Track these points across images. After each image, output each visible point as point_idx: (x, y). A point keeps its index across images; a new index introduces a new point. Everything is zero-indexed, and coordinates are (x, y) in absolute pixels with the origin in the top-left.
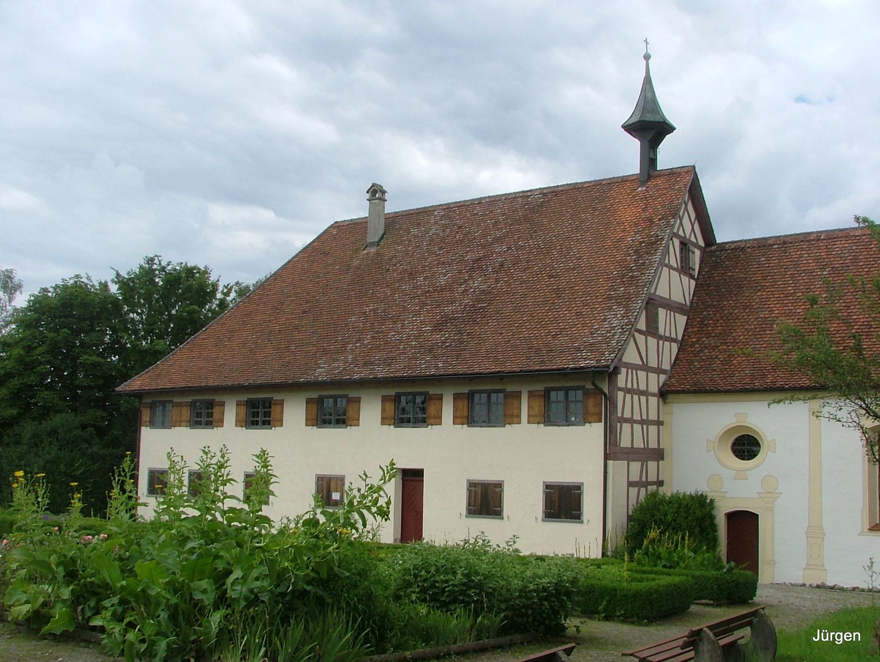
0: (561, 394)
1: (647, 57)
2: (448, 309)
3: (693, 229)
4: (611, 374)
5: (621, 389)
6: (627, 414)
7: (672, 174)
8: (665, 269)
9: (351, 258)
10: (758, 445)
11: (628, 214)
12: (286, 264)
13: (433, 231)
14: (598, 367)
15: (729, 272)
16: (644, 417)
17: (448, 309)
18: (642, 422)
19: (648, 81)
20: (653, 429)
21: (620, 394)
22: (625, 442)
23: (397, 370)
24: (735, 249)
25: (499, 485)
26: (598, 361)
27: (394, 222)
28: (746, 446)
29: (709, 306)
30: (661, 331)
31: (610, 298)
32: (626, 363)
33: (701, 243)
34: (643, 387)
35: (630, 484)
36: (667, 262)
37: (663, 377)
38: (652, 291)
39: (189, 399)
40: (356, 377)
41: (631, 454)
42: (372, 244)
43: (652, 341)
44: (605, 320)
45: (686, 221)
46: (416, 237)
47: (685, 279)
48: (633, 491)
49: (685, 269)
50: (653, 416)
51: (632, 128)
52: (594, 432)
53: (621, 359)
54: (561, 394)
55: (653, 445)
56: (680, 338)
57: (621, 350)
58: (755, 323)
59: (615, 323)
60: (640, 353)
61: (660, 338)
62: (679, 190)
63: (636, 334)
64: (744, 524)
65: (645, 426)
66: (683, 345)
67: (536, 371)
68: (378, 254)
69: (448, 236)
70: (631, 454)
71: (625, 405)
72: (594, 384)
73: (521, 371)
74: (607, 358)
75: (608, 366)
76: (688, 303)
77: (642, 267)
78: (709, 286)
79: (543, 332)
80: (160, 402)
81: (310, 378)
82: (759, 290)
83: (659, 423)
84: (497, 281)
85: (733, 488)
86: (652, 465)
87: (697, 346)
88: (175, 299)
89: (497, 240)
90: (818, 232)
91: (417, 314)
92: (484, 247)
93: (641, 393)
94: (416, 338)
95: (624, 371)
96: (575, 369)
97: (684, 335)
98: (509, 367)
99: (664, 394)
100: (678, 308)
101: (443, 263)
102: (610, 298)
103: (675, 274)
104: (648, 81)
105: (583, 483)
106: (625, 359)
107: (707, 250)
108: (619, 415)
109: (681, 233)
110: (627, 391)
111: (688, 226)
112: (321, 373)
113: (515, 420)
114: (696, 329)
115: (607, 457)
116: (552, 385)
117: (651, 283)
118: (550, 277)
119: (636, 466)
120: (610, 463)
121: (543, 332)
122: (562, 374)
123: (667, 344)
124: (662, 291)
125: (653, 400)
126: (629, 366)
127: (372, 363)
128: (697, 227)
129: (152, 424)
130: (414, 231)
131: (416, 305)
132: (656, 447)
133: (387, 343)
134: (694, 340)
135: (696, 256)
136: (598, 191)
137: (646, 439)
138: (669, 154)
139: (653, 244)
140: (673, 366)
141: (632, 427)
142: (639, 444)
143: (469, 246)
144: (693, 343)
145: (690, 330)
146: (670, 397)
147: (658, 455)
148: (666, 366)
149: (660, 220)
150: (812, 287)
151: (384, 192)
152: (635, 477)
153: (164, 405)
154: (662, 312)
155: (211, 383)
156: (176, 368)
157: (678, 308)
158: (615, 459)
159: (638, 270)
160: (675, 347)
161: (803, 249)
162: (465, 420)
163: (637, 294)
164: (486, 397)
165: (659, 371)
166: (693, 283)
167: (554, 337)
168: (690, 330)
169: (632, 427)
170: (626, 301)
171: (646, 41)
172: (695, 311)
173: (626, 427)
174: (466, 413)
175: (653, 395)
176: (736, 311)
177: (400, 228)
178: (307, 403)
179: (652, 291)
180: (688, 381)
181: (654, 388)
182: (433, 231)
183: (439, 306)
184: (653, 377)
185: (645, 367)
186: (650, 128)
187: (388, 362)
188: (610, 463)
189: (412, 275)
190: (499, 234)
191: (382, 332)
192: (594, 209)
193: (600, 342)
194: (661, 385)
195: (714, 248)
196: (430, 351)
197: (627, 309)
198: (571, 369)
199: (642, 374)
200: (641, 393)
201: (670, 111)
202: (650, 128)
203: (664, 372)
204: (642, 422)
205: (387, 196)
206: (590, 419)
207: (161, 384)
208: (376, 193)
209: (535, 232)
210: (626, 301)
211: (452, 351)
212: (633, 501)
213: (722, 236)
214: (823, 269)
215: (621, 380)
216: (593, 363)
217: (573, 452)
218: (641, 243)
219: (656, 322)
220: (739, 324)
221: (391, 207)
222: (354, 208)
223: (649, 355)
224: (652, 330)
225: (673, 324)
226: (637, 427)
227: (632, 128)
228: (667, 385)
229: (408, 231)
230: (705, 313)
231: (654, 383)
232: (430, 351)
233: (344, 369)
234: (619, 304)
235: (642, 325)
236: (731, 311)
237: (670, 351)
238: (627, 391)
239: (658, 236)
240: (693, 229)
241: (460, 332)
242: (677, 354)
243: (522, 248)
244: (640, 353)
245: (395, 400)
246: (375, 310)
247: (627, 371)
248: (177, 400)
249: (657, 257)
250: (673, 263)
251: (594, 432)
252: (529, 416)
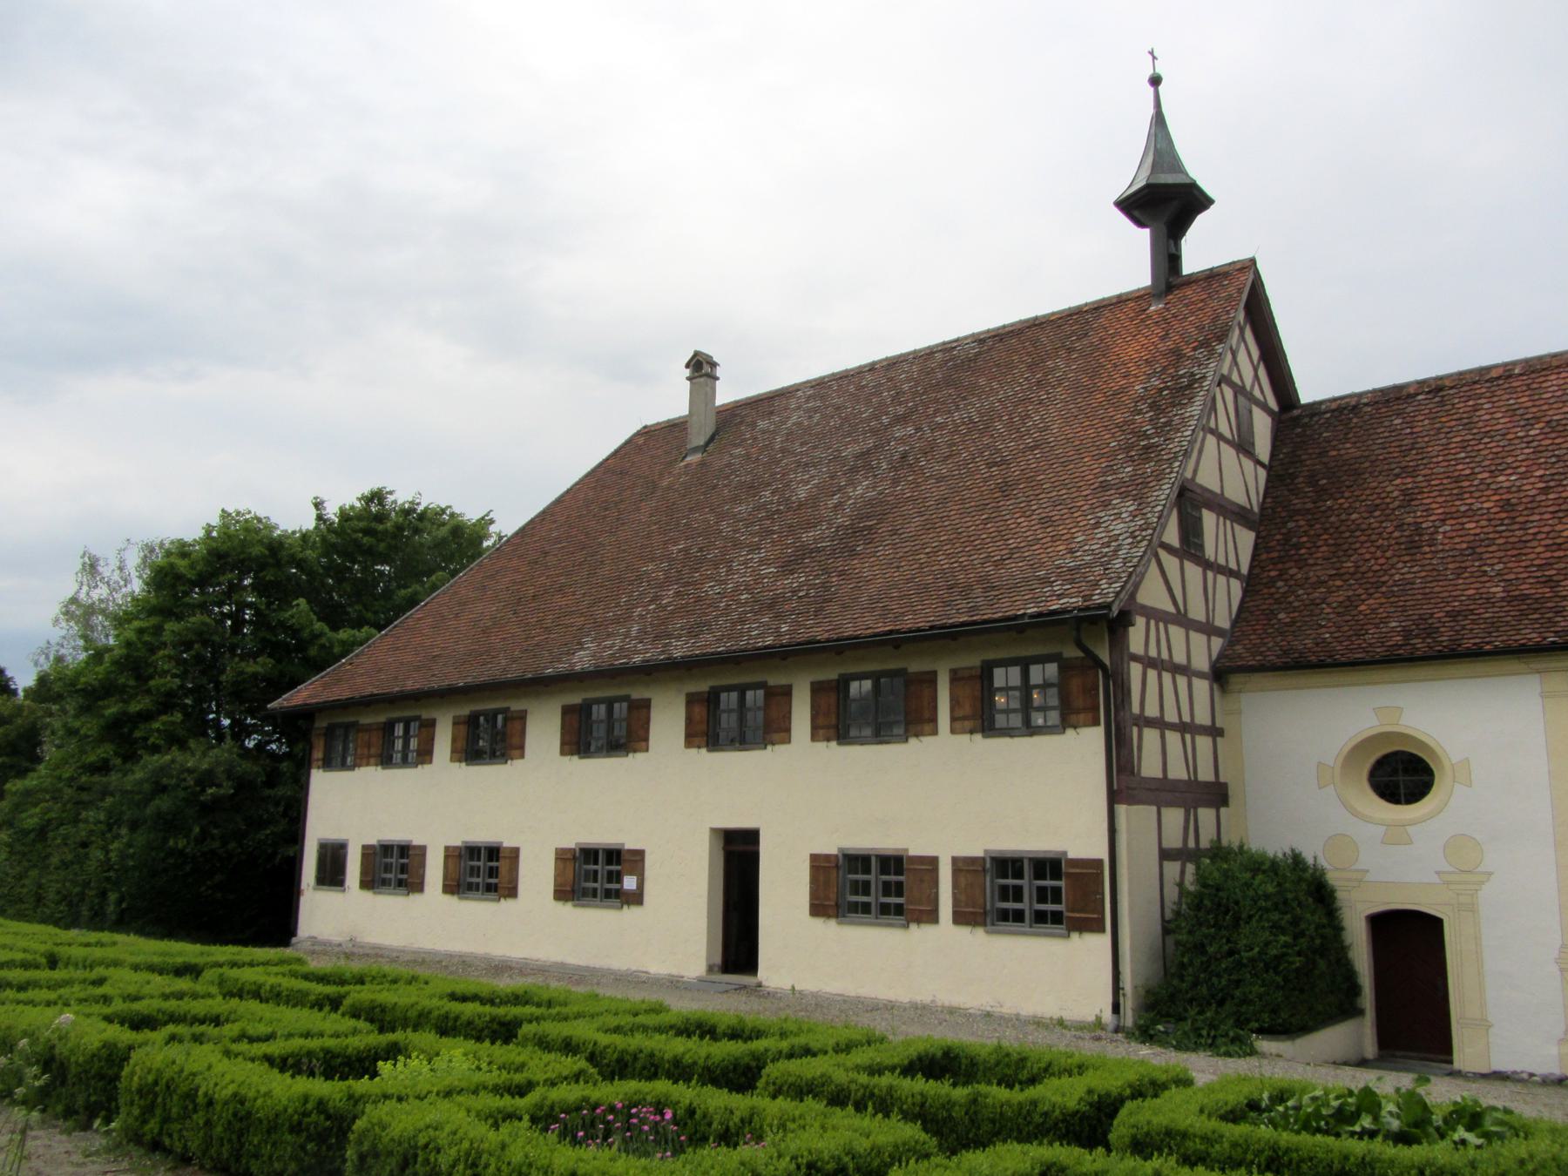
0: (1015, 674)
1: (1155, 81)
2: (808, 537)
3: (1256, 377)
4: (1115, 623)
5: (1135, 658)
6: (1152, 711)
7: (1212, 277)
8: (1211, 441)
9: (661, 475)
10: (1428, 772)
11: (1132, 349)
12: (563, 496)
13: (794, 419)
14: (1088, 608)
15: (1331, 460)
16: (1186, 718)
17: (808, 537)
18: (1183, 728)
19: (1159, 120)
20: (1203, 743)
21: (1135, 670)
22: (1150, 767)
23: (709, 643)
24: (1340, 409)
25: (814, 858)
26: (1086, 598)
27: (735, 418)
28: (1402, 775)
29: (1298, 512)
30: (1209, 552)
31: (1104, 487)
32: (1143, 607)
33: (1272, 403)
34: (1180, 658)
35: (1165, 855)
36: (1212, 424)
37: (1217, 643)
38: (1188, 475)
39: (382, 718)
40: (637, 659)
41: (1163, 792)
42: (695, 450)
43: (1193, 571)
44: (1097, 525)
45: (1242, 357)
46: (764, 432)
47: (1248, 464)
48: (1172, 869)
49: (1244, 446)
50: (1203, 718)
51: (1138, 206)
52: (1085, 747)
53: (1133, 596)
54: (1015, 674)
55: (1205, 775)
56: (1245, 570)
57: (1134, 580)
58: (1396, 534)
59: (1118, 528)
60: (1170, 589)
61: (1207, 565)
62: (1230, 298)
63: (1163, 554)
64: (1412, 941)
65: (1188, 737)
66: (1252, 584)
67: (963, 624)
68: (702, 464)
69: (817, 424)
70: (1163, 792)
71: (1148, 692)
72: (1080, 645)
73: (932, 628)
74: (1106, 592)
75: (1108, 606)
76: (1256, 509)
77: (1167, 429)
78: (1293, 476)
79: (976, 559)
80: (340, 725)
81: (562, 667)
82: (1397, 476)
83: (1215, 732)
84: (895, 482)
85: (1379, 861)
86: (1206, 815)
87: (1280, 584)
88: (383, 557)
89: (902, 420)
90: (1505, 365)
91: (756, 548)
92: (874, 432)
93: (1177, 669)
94: (748, 589)
95: (1140, 621)
96: (1040, 615)
97: (1251, 567)
98: (909, 622)
99: (1220, 675)
100: (1239, 515)
101: (806, 465)
102: (1104, 487)
103: (1229, 452)
104: (1159, 120)
105: (715, 831)
106: (1144, 598)
107: (1285, 417)
108: (1136, 709)
109: (1235, 378)
110: (1149, 663)
111: (1246, 364)
112: (582, 660)
113: (927, 727)
114: (1275, 554)
115: (1114, 797)
116: (991, 655)
117: (1187, 454)
118: (989, 466)
119: (1174, 817)
120: (1121, 809)
121: (976, 559)
122: (1015, 627)
123: (1221, 579)
124: (1207, 478)
125: (1202, 687)
126: (1152, 614)
127: (670, 636)
128: (1262, 372)
129: (328, 764)
130: (763, 424)
131: (753, 534)
132: (1164, 811)
133: (698, 600)
134: (1273, 574)
135: (1262, 426)
136: (1076, 322)
137: (1191, 762)
138: (1202, 249)
139: (1183, 391)
140: (1234, 623)
141: (1163, 737)
142: (1178, 772)
143: (849, 435)
144: (1273, 581)
145: (1264, 556)
146: (1236, 680)
147: (1218, 795)
148: (1223, 621)
149: (1194, 349)
150: (1509, 460)
151: (714, 365)
152: (1173, 840)
153: (385, 731)
154: (1209, 519)
155: (411, 685)
156: (374, 663)
157: (1239, 515)
158: (1132, 800)
159: (1157, 434)
160: (1236, 587)
161: (1480, 396)
162: (832, 732)
163: (1159, 476)
164: (876, 692)
165: (1208, 629)
166: (1262, 473)
167: (997, 564)
168: (1264, 556)
169: (1163, 737)
170: (1137, 490)
171: (1151, 53)
172: (1267, 519)
173: (1151, 736)
174: (834, 721)
175: (1200, 675)
176: (1354, 516)
177: (741, 423)
178: (454, 724)
179: (1188, 475)
180: (1276, 642)
181: (1201, 662)
182: (794, 419)
183: (811, 555)
184: (1198, 639)
185: (1181, 618)
186: (1166, 204)
187: (693, 632)
188: (1121, 809)
189: (752, 488)
190: (901, 410)
191: (694, 583)
192: (1070, 350)
193: (1088, 565)
194: (1214, 657)
195: (1296, 412)
196: (771, 606)
197: (1140, 499)
198: (1032, 616)
199: (1176, 632)
200: (1177, 669)
201: (1199, 168)
202: (1166, 204)
203: (1219, 632)
204: (1183, 728)
205: (719, 372)
206: (1073, 718)
207: (341, 692)
208: (701, 368)
209: (964, 399)
210: (1137, 490)
211: (809, 604)
212: (1172, 893)
213: (1311, 387)
214: (1529, 424)
215: (1136, 638)
216: (1076, 601)
217: (1041, 791)
218: (1161, 390)
219: (1199, 533)
220: (1363, 538)
221: (726, 394)
222: (670, 400)
223: (1187, 599)
224: (1190, 546)
225: (1230, 544)
226: (1173, 738)
227: (1138, 206)
228: (1226, 656)
229: (754, 425)
230: (1291, 525)
231: (1202, 652)
232: (771, 606)
233: (621, 648)
234: (1124, 496)
235: (1172, 535)
236: (1344, 517)
237: (1227, 597)
238: (1149, 663)
239: (1193, 374)
240: (1256, 377)
241: (826, 571)
242: (1242, 602)
243: (941, 427)
244: (1170, 589)
245: (708, 700)
246: (686, 550)
247: (1148, 624)
248: (366, 720)
249: (1195, 409)
250: (1224, 429)
251: (1085, 747)
252: (953, 719)
